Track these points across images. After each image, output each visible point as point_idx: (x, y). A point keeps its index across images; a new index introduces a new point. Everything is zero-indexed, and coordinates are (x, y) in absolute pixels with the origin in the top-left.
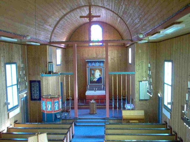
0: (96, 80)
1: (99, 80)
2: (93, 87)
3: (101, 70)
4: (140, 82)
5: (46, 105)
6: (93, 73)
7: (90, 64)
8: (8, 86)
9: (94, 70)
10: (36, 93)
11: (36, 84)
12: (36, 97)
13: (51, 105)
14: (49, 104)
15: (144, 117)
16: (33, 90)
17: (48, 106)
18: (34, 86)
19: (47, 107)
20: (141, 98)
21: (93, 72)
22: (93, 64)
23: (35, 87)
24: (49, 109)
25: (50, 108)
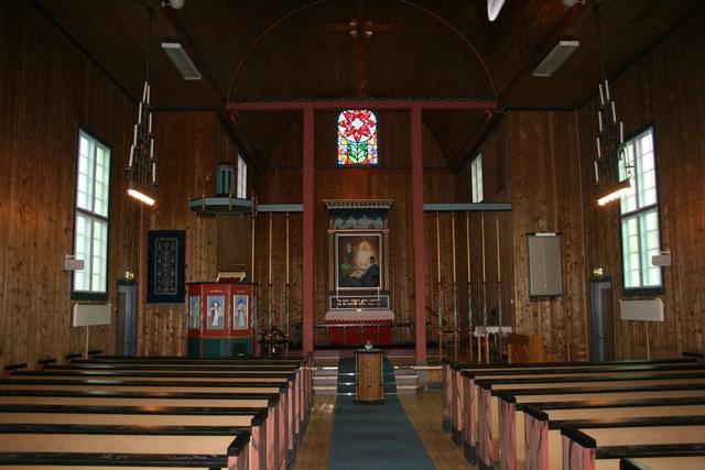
0: (359, 274)
1: (372, 277)
2: (350, 299)
3: (374, 242)
4: (531, 239)
5: (204, 309)
6: (349, 250)
7: (339, 221)
8: (90, 209)
9: (355, 241)
10: (169, 275)
11: (170, 242)
12: (169, 288)
13: (222, 309)
14: (216, 305)
15: (512, 467)
16: (158, 253)
17: (213, 312)
18: (164, 249)
19: (209, 314)
20: (533, 293)
21: (349, 248)
22: (351, 221)
23: (166, 253)
24: (215, 323)
25: (220, 318)
